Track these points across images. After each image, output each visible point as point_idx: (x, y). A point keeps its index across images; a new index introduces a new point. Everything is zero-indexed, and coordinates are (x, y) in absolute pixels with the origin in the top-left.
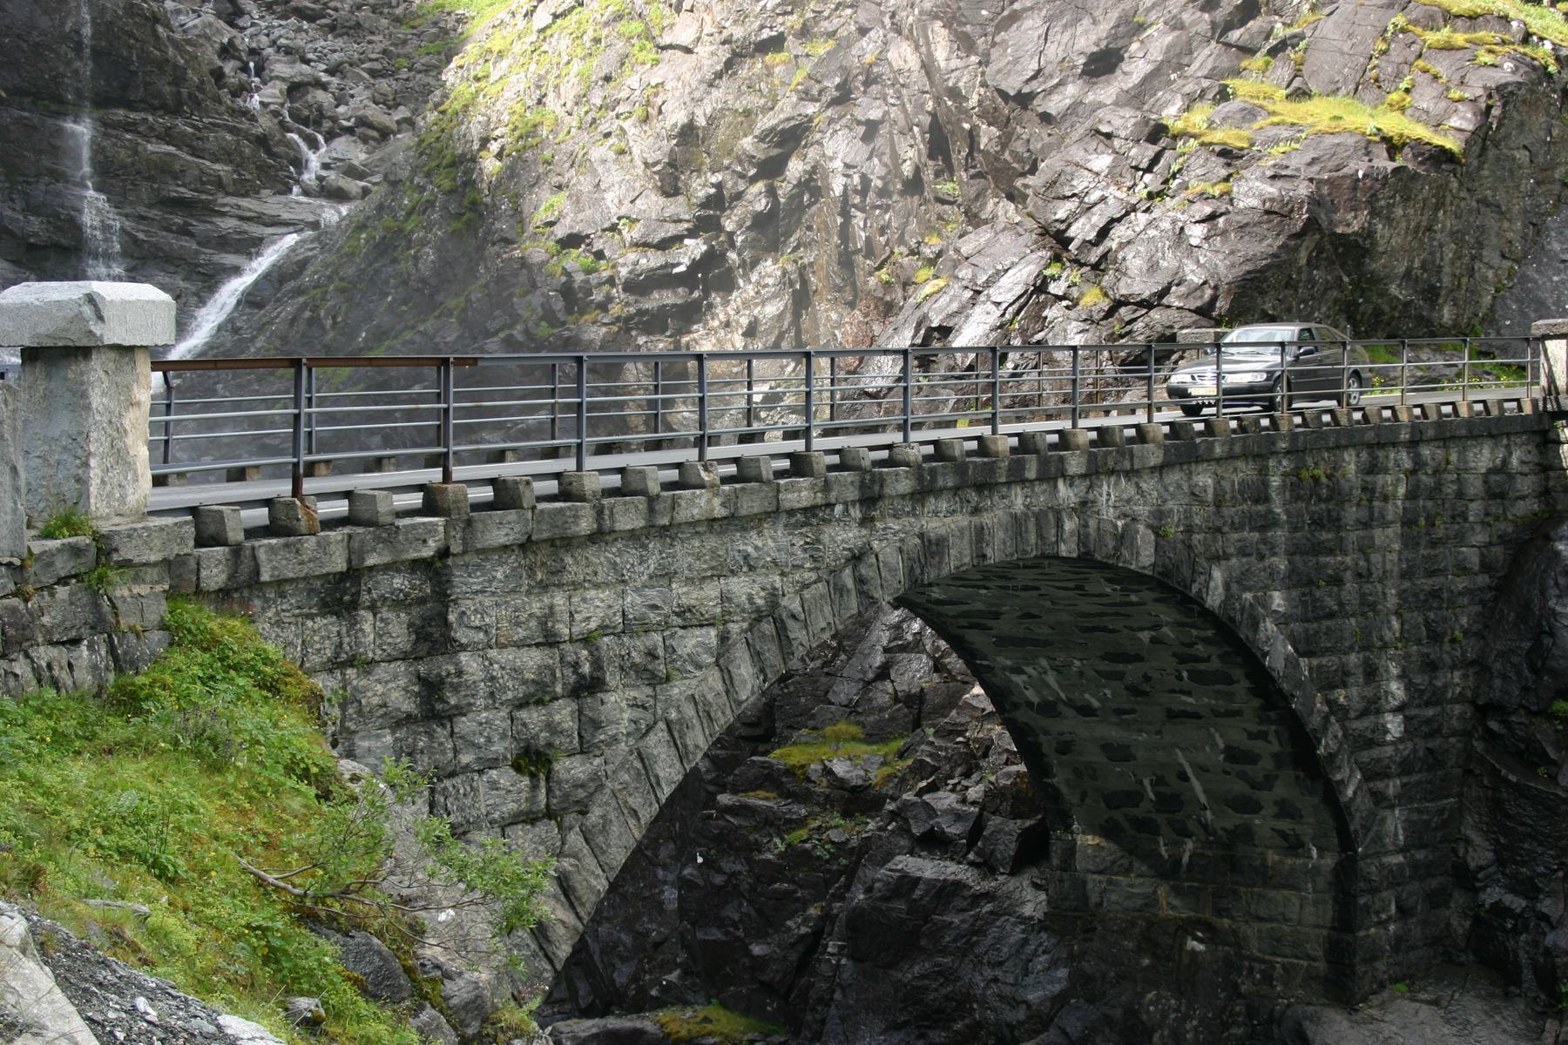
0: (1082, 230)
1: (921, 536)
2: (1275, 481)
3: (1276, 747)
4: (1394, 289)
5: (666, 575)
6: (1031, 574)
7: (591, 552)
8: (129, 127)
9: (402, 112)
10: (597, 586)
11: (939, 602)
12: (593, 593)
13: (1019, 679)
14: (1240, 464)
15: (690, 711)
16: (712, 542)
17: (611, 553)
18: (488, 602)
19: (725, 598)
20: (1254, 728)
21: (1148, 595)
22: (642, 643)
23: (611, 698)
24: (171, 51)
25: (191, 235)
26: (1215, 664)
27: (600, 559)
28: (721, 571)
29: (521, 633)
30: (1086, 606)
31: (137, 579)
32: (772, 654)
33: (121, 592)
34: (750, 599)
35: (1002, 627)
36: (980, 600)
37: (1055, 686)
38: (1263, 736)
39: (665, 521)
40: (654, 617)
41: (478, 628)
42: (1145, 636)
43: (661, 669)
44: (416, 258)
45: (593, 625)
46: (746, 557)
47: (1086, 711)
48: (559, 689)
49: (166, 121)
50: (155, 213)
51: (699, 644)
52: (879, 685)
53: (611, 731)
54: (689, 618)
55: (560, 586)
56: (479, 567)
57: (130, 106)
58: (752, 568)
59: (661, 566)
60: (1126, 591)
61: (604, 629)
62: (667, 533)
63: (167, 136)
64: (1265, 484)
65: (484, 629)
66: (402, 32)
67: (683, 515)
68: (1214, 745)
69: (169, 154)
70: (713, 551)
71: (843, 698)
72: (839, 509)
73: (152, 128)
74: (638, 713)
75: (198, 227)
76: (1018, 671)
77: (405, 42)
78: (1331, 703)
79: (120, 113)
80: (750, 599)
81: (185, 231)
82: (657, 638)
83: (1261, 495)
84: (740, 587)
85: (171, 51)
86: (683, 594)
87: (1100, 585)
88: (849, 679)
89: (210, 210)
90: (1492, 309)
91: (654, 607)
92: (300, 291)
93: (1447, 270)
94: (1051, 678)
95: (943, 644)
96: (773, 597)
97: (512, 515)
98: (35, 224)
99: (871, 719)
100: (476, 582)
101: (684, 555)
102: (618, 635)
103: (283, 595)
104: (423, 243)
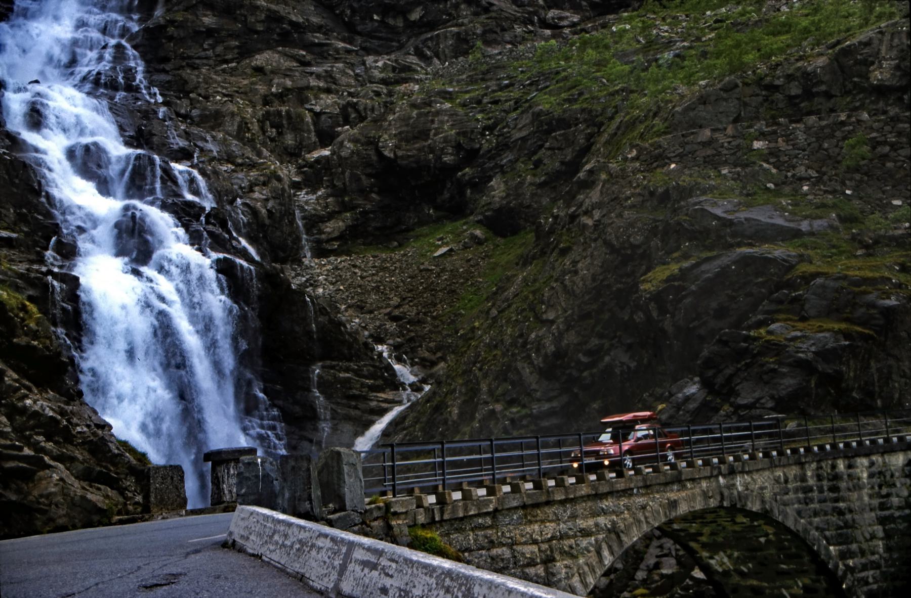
0: (720, 380)
1: (668, 499)
2: (809, 474)
3: (824, 585)
4: (854, 394)
5: (574, 517)
6: (713, 515)
7: (546, 509)
8: (333, 367)
9: (439, 354)
10: (550, 521)
11: (677, 530)
12: (548, 524)
13: (712, 562)
14: (794, 467)
15: (586, 568)
16: (589, 504)
17: (554, 509)
18: (511, 528)
19: (597, 525)
20: (814, 577)
21: (761, 522)
22: (567, 542)
23: (558, 564)
24: (347, 337)
25: (359, 409)
26: (794, 550)
27: (550, 511)
28: (594, 514)
29: (524, 539)
30: (737, 528)
31: (399, 519)
32: (616, 548)
33: (393, 523)
34: (605, 525)
35: (704, 539)
36: (694, 528)
37: (728, 564)
38: (818, 581)
39: (572, 496)
40: (571, 533)
41: (509, 538)
42: (762, 540)
43: (575, 553)
44: (450, 412)
45: (549, 536)
46: (603, 509)
47: (742, 574)
48: (538, 561)
49: (347, 364)
50: (344, 401)
51: (589, 543)
52: (655, 572)
53: (559, 577)
54: (586, 533)
55: (536, 521)
56: (507, 515)
57: (333, 360)
58: (605, 514)
59: (572, 514)
60: (752, 521)
61: (553, 538)
62: (573, 501)
63: (347, 370)
64: (805, 475)
65: (511, 538)
66: (437, 323)
67: (578, 494)
68: (798, 586)
69: (348, 378)
70: (590, 507)
71: (640, 578)
72: (635, 491)
73: (341, 368)
74: (568, 570)
75: (361, 405)
76: (711, 558)
77: (438, 326)
78: (847, 566)
79: (328, 363)
80: (605, 525)
81: (356, 408)
82: (573, 541)
83: (803, 479)
84: (602, 520)
85: (347, 337)
86: (582, 523)
87: (741, 519)
88: (643, 570)
89: (366, 399)
90: (900, 399)
91: (570, 529)
92: (404, 429)
93: (877, 384)
94: (726, 560)
95: (678, 547)
96: (614, 523)
97: (518, 496)
98: (297, 409)
99: (653, 586)
100: (507, 520)
101: (580, 508)
102: (559, 540)
103: (442, 526)
104: (453, 406)
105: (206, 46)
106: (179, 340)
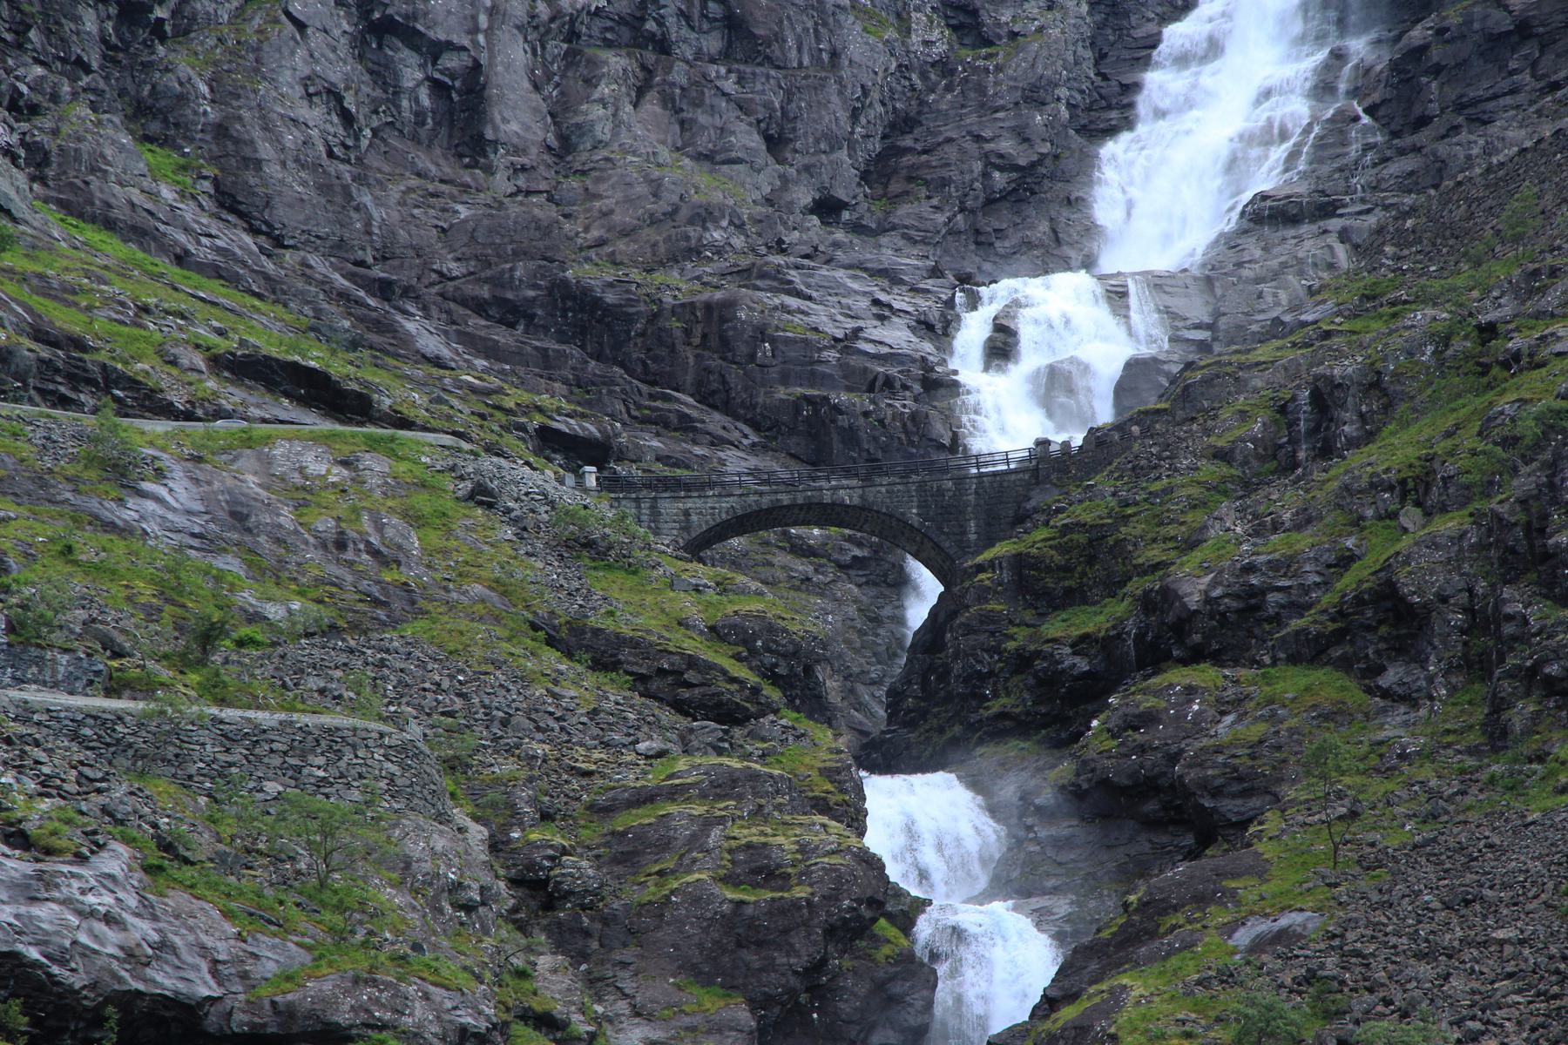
105: (1513, 65)
106: (950, 419)
